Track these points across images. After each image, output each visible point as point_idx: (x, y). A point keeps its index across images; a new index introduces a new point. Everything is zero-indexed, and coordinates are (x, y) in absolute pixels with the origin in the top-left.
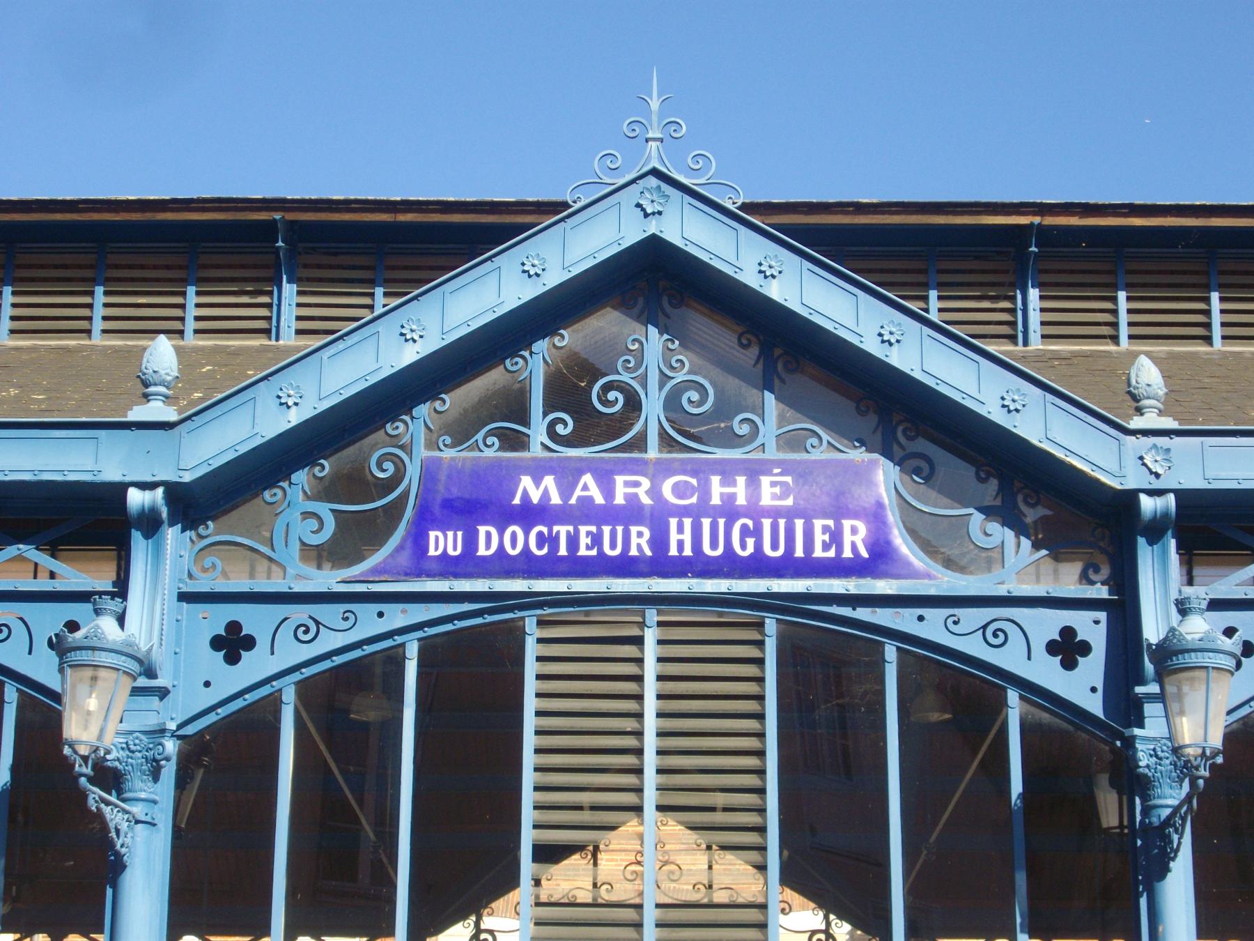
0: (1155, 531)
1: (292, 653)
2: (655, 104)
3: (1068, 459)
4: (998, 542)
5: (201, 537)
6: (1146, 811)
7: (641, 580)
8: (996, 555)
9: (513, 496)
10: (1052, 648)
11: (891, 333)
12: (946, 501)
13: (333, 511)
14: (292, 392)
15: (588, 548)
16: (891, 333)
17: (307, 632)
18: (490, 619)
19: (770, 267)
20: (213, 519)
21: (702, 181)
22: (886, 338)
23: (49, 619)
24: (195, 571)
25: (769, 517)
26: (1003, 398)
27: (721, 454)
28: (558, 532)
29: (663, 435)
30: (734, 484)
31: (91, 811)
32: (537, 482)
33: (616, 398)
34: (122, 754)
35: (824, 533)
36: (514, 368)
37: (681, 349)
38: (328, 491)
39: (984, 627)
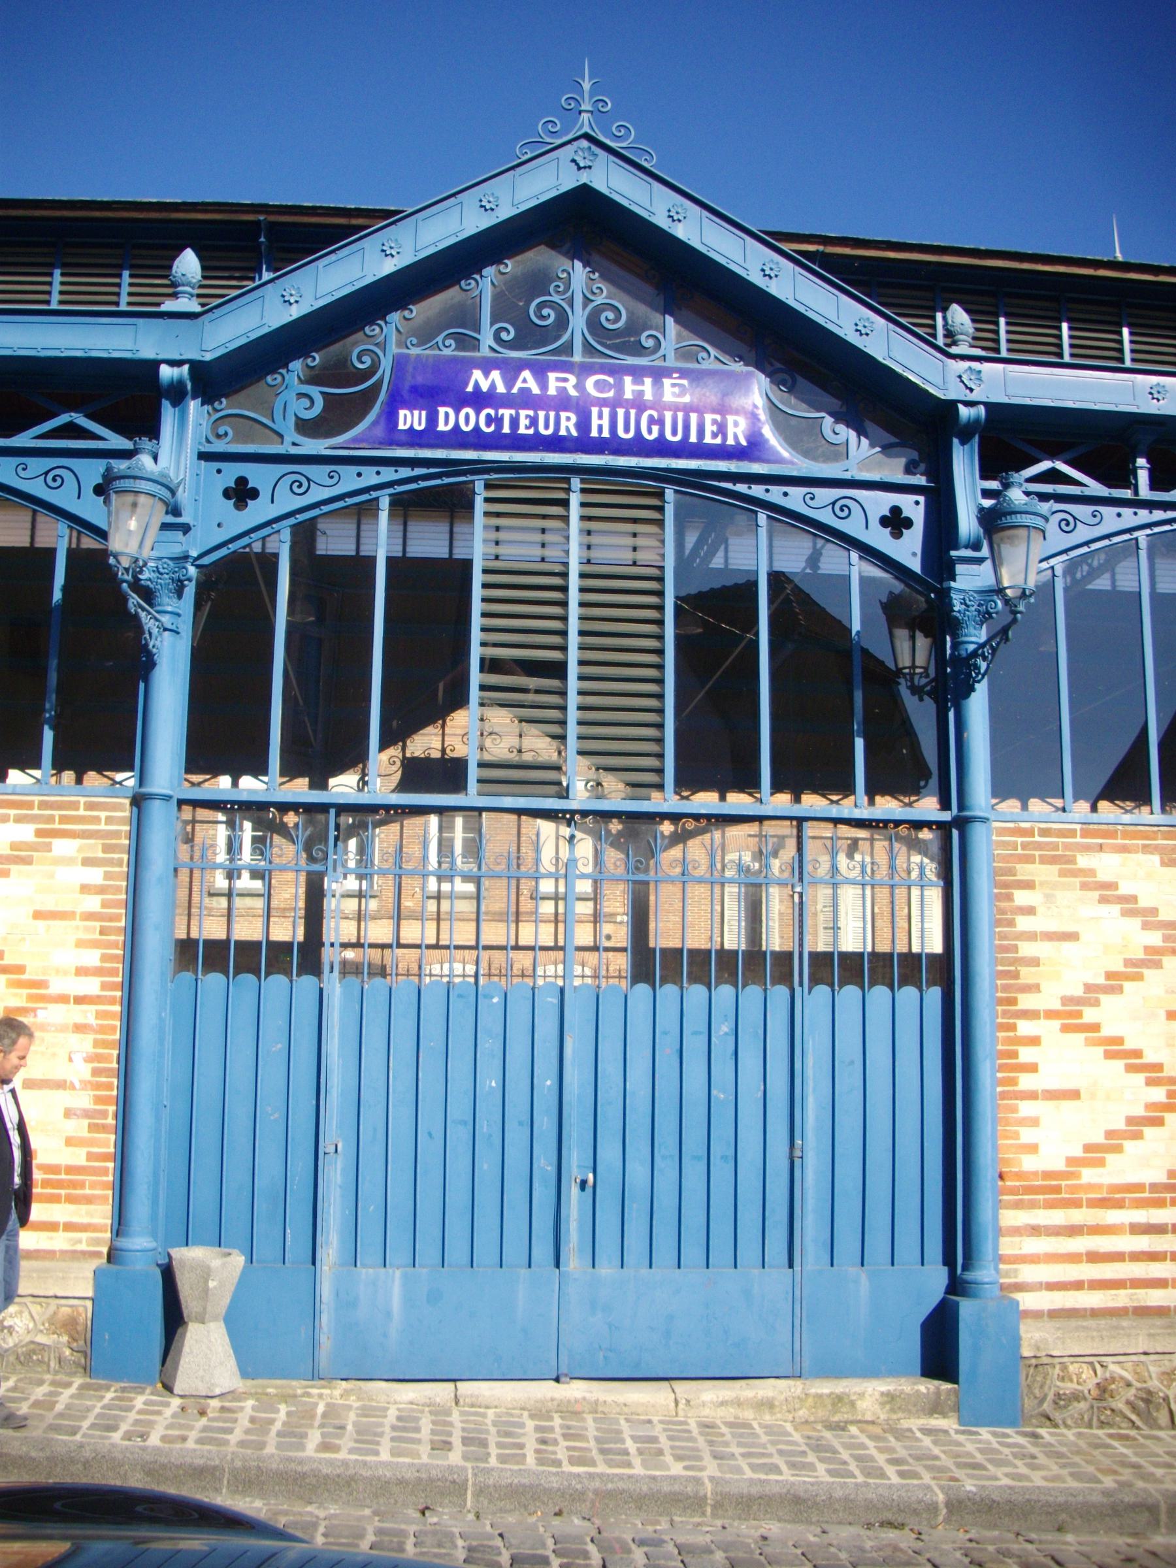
0: (966, 433)
1: (288, 502)
2: (586, 85)
3: (905, 374)
4: (844, 440)
5: (217, 411)
6: (955, 646)
7: (568, 455)
8: (843, 449)
9: (467, 384)
10: (884, 521)
11: (771, 269)
12: (804, 406)
13: (322, 393)
14: (293, 292)
15: (527, 428)
16: (771, 269)
17: (300, 486)
18: (447, 480)
19: (678, 213)
20: (226, 396)
21: (624, 145)
22: (767, 273)
23: (93, 471)
24: (212, 438)
25: (670, 410)
26: (856, 325)
27: (631, 361)
28: (503, 415)
29: (586, 344)
30: (643, 383)
31: (130, 613)
32: (486, 374)
33: (549, 315)
34: (154, 576)
35: (713, 425)
36: (468, 288)
37: (600, 280)
39: (834, 504)
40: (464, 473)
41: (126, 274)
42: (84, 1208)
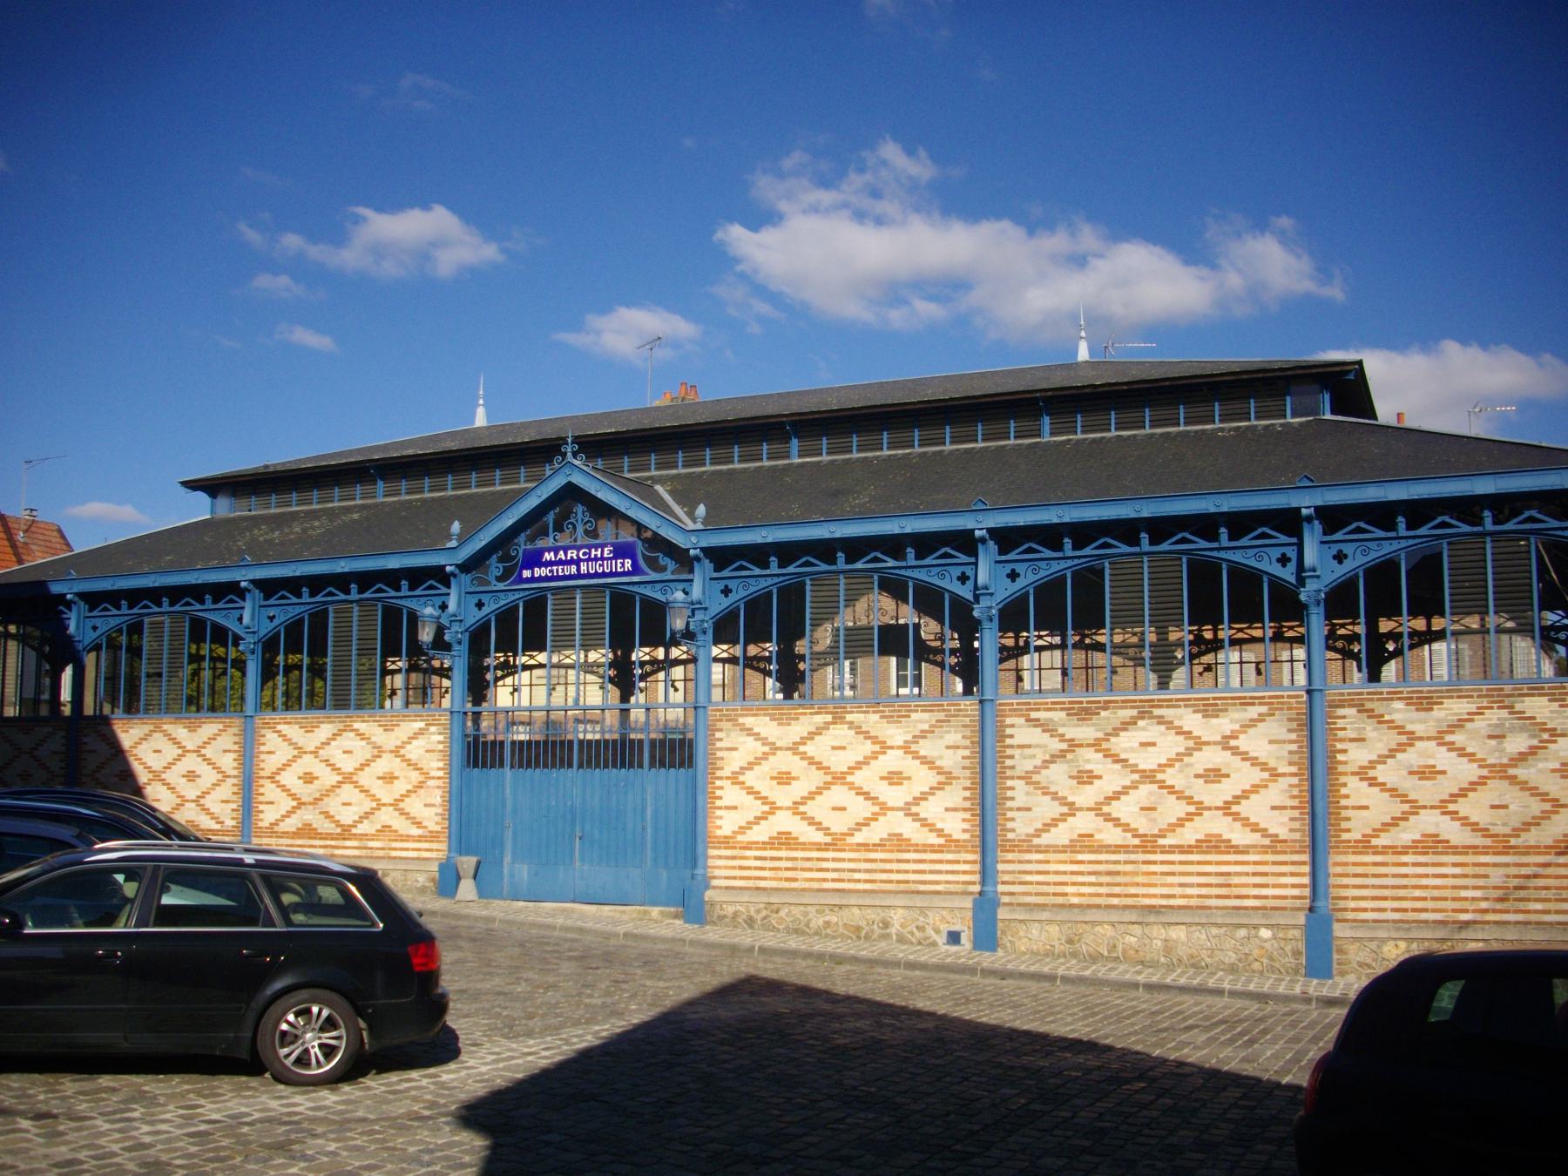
10: (1278, 560)
38: (500, 560)
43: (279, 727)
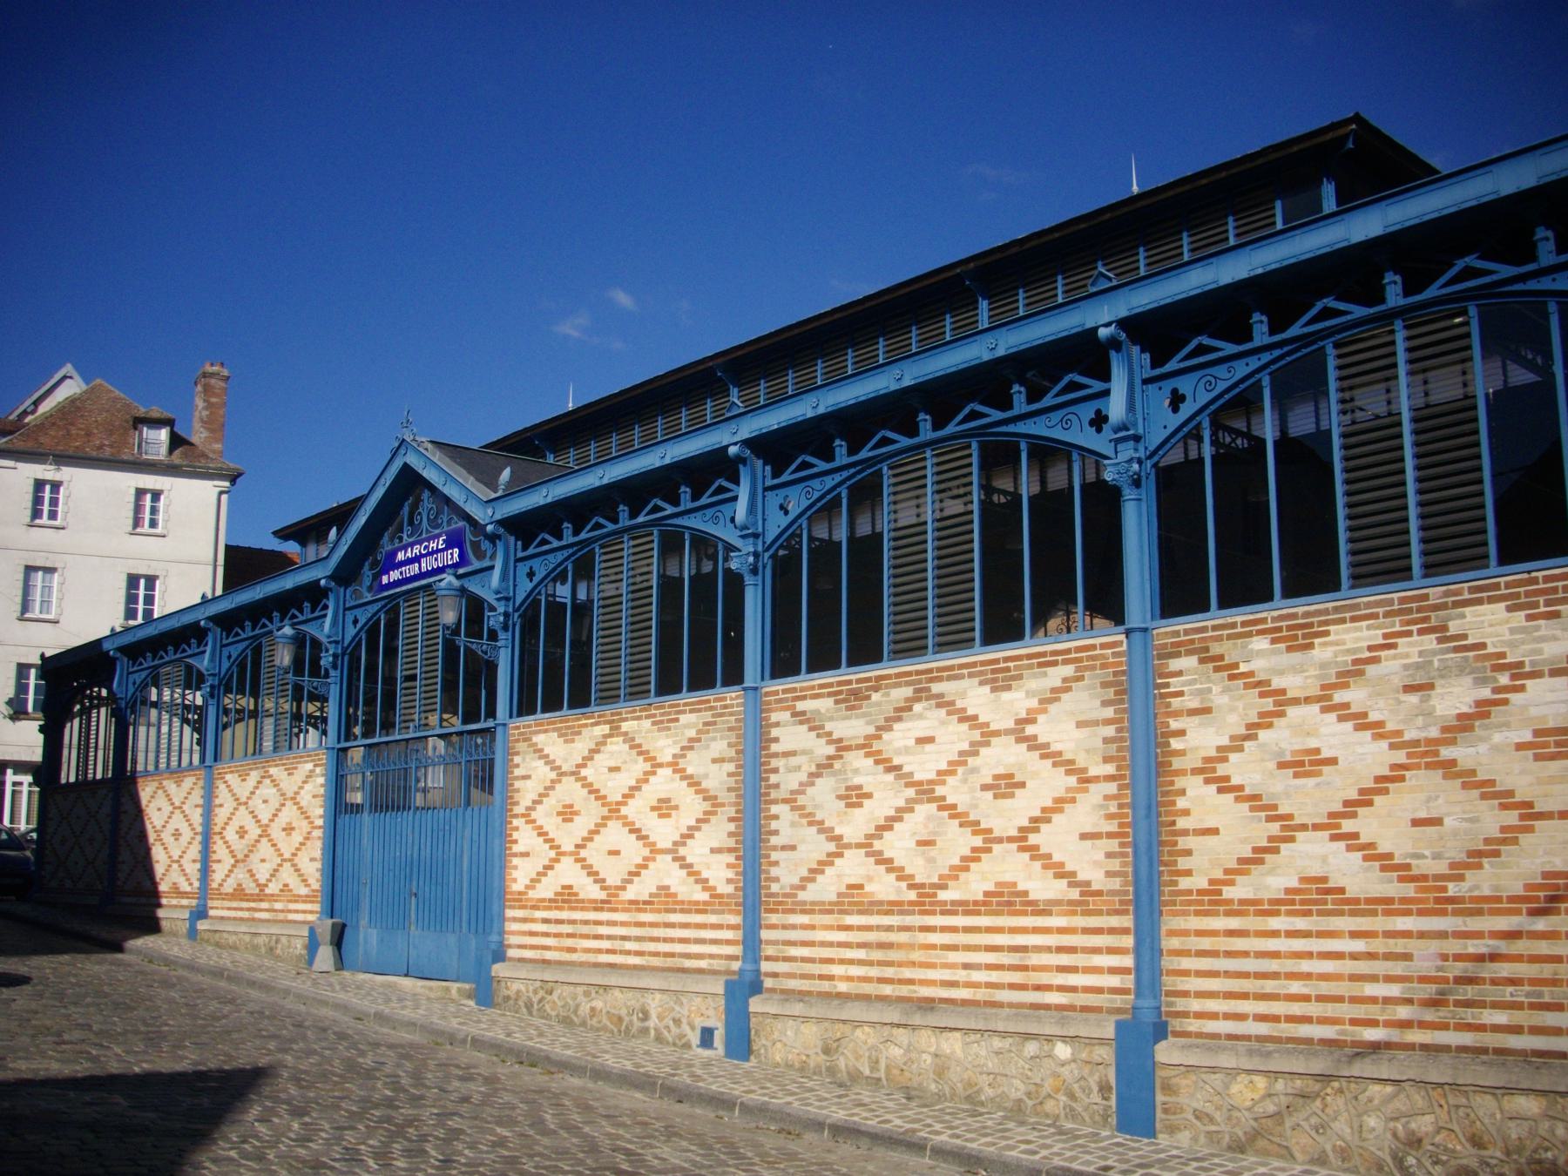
1: (1203, 398)
40: (875, 465)
41: (1230, 219)
42: (1333, 984)
43: (228, 777)
